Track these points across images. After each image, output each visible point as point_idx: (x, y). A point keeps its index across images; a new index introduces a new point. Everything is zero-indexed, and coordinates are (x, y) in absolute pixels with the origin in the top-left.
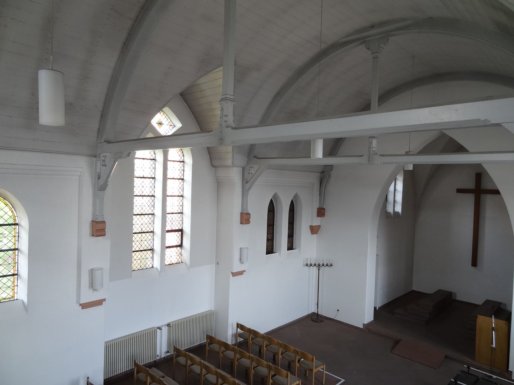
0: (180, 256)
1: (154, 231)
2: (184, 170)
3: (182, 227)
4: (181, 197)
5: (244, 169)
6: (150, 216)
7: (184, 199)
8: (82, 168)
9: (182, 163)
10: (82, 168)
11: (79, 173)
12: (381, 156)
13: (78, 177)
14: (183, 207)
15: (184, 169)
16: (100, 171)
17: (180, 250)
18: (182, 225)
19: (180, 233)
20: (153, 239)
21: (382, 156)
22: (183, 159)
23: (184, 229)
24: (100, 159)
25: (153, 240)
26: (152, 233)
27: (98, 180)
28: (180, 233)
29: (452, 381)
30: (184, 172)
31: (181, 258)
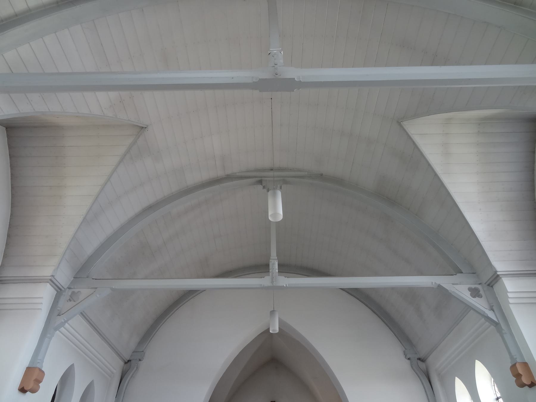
5: (59, 291)
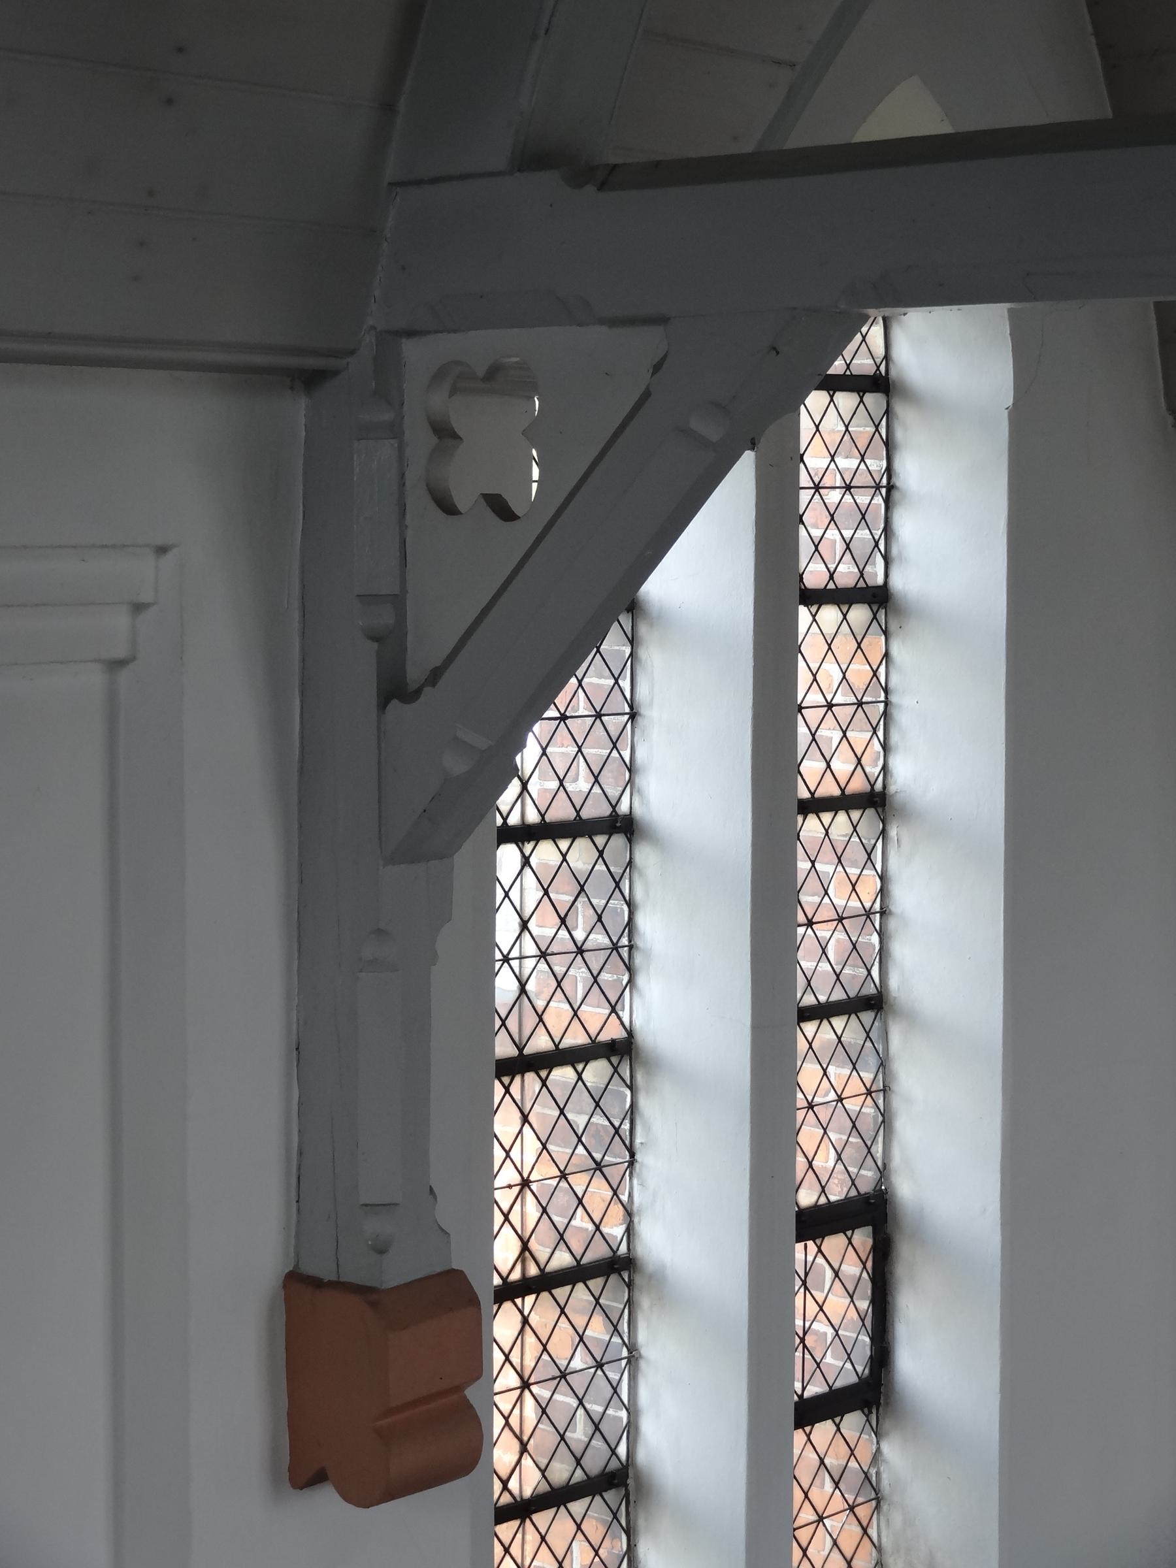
0: (863, 1512)
1: (640, 1251)
2: (890, 488)
3: (883, 1171)
4: (870, 812)
6: (596, 1072)
7: (893, 832)
8: (162, 550)
9: (874, 400)
10: (162, 550)
11: (121, 620)
12: (590, 190)
13: (95, 679)
14: (893, 924)
15: (889, 470)
16: (397, 591)
17: (869, 1438)
18: (878, 1150)
19: (863, 1238)
20: (632, 1348)
21: (602, 186)
22: (880, 351)
23: (905, 1189)
24: (387, 416)
25: (634, 1358)
26: (613, 1278)
27: (383, 705)
28: (863, 1238)
29: (615, 1480)
30: (887, 501)
31: (873, 1532)
